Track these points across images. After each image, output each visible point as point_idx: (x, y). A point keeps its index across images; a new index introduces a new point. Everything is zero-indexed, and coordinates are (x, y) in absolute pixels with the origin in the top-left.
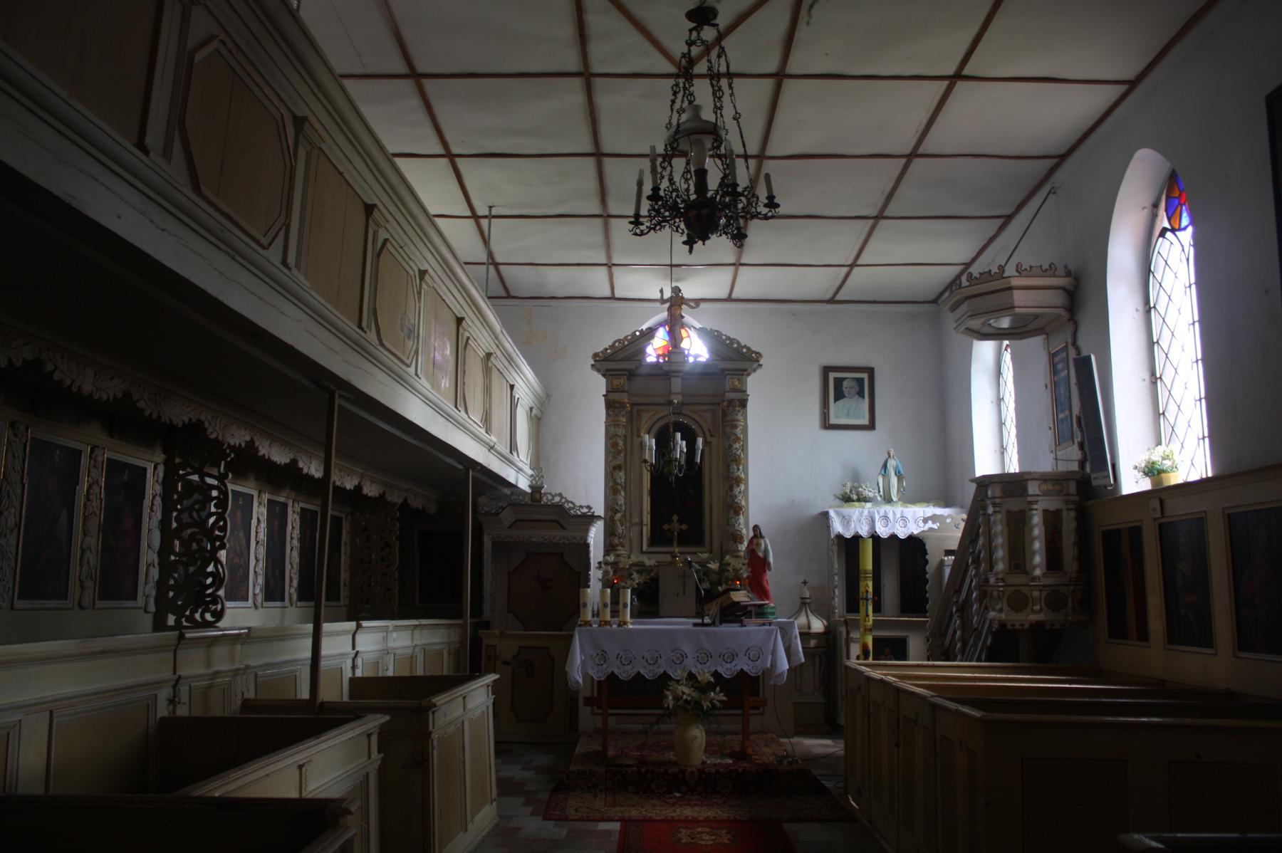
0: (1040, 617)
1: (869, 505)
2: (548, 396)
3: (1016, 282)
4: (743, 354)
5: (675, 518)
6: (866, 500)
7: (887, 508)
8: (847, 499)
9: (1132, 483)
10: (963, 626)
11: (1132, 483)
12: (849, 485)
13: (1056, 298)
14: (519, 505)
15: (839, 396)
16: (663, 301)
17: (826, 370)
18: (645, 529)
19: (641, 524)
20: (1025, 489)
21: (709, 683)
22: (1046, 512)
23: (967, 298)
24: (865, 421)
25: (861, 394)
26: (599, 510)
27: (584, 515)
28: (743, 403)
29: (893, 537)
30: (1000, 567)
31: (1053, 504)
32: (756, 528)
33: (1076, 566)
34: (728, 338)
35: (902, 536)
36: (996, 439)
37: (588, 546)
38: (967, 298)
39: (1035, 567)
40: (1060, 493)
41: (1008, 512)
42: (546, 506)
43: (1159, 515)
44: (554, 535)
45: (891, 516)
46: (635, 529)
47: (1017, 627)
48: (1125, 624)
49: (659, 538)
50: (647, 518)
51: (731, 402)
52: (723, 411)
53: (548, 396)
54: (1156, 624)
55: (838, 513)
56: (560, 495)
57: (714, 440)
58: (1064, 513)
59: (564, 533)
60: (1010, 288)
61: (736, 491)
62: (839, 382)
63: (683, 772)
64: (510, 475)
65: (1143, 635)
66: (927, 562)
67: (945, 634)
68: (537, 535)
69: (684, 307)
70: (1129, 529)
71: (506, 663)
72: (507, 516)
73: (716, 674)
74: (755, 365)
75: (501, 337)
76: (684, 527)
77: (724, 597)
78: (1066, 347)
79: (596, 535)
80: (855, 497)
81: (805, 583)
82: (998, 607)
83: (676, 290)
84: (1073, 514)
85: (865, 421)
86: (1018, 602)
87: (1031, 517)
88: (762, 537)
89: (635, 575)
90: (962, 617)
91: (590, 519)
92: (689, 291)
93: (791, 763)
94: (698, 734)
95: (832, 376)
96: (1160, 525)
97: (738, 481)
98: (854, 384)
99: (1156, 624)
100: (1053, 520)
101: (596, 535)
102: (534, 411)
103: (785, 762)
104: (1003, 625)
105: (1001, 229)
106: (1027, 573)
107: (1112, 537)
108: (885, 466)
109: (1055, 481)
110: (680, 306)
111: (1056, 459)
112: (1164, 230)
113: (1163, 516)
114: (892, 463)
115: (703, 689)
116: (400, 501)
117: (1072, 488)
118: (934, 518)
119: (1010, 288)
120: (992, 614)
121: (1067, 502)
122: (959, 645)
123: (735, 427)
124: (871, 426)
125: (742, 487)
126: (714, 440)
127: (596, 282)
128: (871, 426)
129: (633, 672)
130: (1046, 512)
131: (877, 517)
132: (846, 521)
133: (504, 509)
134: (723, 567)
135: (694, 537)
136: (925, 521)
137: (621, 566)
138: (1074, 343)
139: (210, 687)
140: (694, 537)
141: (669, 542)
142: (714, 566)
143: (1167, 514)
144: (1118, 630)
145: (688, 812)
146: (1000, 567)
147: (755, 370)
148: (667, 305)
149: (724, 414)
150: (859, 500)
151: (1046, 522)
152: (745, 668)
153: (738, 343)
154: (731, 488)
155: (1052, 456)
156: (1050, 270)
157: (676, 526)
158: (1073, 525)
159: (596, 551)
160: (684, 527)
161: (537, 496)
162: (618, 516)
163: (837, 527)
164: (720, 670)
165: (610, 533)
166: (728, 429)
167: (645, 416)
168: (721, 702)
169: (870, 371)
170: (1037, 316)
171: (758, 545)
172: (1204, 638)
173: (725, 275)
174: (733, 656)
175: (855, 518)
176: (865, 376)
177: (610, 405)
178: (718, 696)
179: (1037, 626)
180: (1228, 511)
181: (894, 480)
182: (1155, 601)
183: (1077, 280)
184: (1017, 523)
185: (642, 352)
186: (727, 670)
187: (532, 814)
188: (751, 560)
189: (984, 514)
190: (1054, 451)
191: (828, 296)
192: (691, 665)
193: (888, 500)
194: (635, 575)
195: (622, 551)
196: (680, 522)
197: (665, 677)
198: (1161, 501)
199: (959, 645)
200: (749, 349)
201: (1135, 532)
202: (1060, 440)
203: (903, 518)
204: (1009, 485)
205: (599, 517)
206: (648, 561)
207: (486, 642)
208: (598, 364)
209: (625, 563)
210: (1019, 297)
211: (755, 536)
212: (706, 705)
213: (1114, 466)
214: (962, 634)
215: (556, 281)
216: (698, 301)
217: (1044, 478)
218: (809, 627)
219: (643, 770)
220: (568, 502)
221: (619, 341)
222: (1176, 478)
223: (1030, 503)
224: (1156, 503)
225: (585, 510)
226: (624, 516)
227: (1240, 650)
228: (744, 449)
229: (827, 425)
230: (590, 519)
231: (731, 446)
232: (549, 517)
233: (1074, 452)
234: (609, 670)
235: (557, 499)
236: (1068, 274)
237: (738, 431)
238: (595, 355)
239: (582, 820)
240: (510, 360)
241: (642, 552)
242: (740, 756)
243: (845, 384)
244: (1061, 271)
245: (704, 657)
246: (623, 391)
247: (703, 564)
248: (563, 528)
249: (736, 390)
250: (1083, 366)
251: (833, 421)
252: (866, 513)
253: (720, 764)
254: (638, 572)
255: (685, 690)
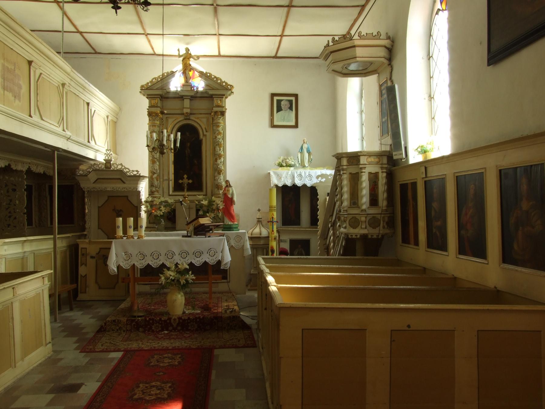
0: (365, 232)
1: (292, 168)
2: (120, 109)
3: (357, 43)
4: (223, 86)
5: (185, 176)
6: (290, 166)
7: (302, 171)
8: (281, 165)
9: (414, 158)
10: (334, 234)
11: (414, 158)
12: (282, 158)
13: (382, 52)
14: (98, 170)
15: (279, 109)
16: (180, 56)
17: (273, 95)
18: (171, 182)
19: (169, 180)
20: (359, 161)
21: (186, 269)
22: (370, 173)
23: (332, 52)
24: (293, 123)
25: (291, 108)
26: (144, 171)
27: (135, 176)
28: (223, 113)
29: (305, 186)
30: (346, 204)
31: (373, 169)
32: (227, 182)
33: (385, 203)
34: (215, 77)
35: (309, 185)
36: (358, 134)
37: (139, 192)
38: (332, 52)
39: (362, 205)
40: (377, 163)
41: (350, 173)
42: (113, 170)
43: (424, 176)
44: (119, 186)
45: (303, 174)
46: (166, 183)
47: (354, 237)
48: (409, 237)
49: (178, 187)
50: (172, 177)
51: (216, 112)
52: (213, 118)
53: (120, 109)
54: (422, 236)
55: (275, 173)
56: (121, 164)
57: (208, 134)
58: (380, 174)
59: (124, 185)
60: (354, 46)
61: (219, 161)
62: (279, 102)
63: (170, 319)
64: (90, 154)
65: (417, 243)
66: (318, 200)
67: (327, 238)
68: (110, 187)
69: (191, 59)
70: (412, 183)
71: (92, 257)
72: (93, 177)
73: (191, 264)
74: (230, 92)
75: (72, 74)
76: (190, 181)
77: (196, 221)
78: (387, 80)
79: (143, 187)
80: (284, 165)
81: (259, 210)
82: (344, 226)
83: (187, 50)
84: (385, 175)
85: (293, 123)
86: (354, 223)
87: (361, 176)
88: (230, 186)
89: (163, 208)
90: (333, 230)
91: (138, 178)
92: (193, 52)
93: (231, 312)
94: (179, 299)
95: (276, 98)
96: (425, 181)
97: (220, 156)
98: (287, 103)
99: (422, 236)
100: (374, 179)
101: (143, 187)
102: (110, 118)
103: (228, 311)
104: (346, 235)
105: (360, 14)
106: (359, 207)
107: (404, 187)
108: (302, 148)
109: (380, 155)
110: (189, 59)
111: (381, 144)
112: (439, 10)
113: (426, 177)
114: (305, 146)
115: (183, 272)
116: (24, 169)
117: (385, 160)
118: (322, 176)
119: (354, 46)
120: (342, 230)
121: (382, 168)
122: (332, 244)
123: (218, 126)
124: (296, 126)
125: (222, 159)
126: (208, 134)
127: (140, 44)
128: (296, 126)
129: (145, 264)
130: (370, 173)
131: (296, 175)
132: (279, 177)
133: (90, 172)
134: (211, 203)
135: (197, 185)
136: (318, 177)
137: (155, 203)
138: (391, 78)
139: (24, 256)
140: (197, 185)
141: (182, 190)
142: (205, 203)
143: (429, 175)
144: (406, 240)
145: (166, 344)
146: (346, 204)
147: (230, 95)
148: (181, 59)
149: (213, 119)
150: (287, 166)
151: (370, 179)
152: (207, 260)
153: (221, 80)
154: (216, 160)
155: (379, 142)
156: (378, 36)
157: (186, 181)
158: (384, 181)
159: (144, 195)
160: (190, 181)
161: (108, 165)
162: (155, 176)
163: (275, 181)
164: (193, 262)
165: (151, 185)
166: (215, 128)
167: (170, 121)
168: (192, 279)
169: (296, 96)
170: (371, 63)
171: (228, 191)
172: (443, 247)
173: (213, 41)
174: (201, 253)
175: (284, 176)
176: (293, 99)
177: (150, 114)
178: (191, 277)
179: (364, 237)
180: (457, 175)
181: (306, 155)
182: (422, 224)
183: (393, 42)
184: (355, 178)
185: (168, 84)
186: (198, 262)
187: (76, 349)
188: (224, 199)
189: (340, 175)
190: (380, 140)
191: (273, 54)
192: (177, 259)
193: (304, 167)
194: (163, 208)
195: (156, 194)
196: (188, 178)
197: (163, 266)
198: (426, 168)
199: (332, 244)
200: (226, 83)
201: (414, 185)
202: (383, 133)
203: (310, 175)
204: (354, 158)
205: (144, 177)
206: (171, 200)
207: (81, 246)
208: (142, 91)
209: (157, 201)
210: (359, 52)
211: (227, 186)
212: (183, 282)
213: (406, 148)
214: (334, 238)
215: (119, 43)
216: (198, 57)
217: (369, 155)
218: (261, 234)
219: (148, 319)
220: (126, 168)
221: (155, 78)
222: (433, 155)
223: (361, 168)
224: (423, 169)
225: (135, 173)
226: (159, 176)
227: (460, 253)
228: (224, 138)
229: (273, 126)
230: (138, 178)
231: (216, 137)
232: (113, 176)
233: (388, 140)
234: (132, 263)
235: (120, 167)
236: (388, 38)
237: (220, 129)
238: (142, 86)
239: (102, 351)
240: (84, 88)
241: (169, 195)
242: (206, 308)
243: (282, 103)
244: (383, 36)
245: (184, 254)
246: (157, 107)
247: (199, 201)
248: (124, 183)
249: (218, 106)
250: (391, 91)
251: (276, 123)
252: (290, 173)
253: (192, 314)
254: (165, 206)
255: (171, 274)
